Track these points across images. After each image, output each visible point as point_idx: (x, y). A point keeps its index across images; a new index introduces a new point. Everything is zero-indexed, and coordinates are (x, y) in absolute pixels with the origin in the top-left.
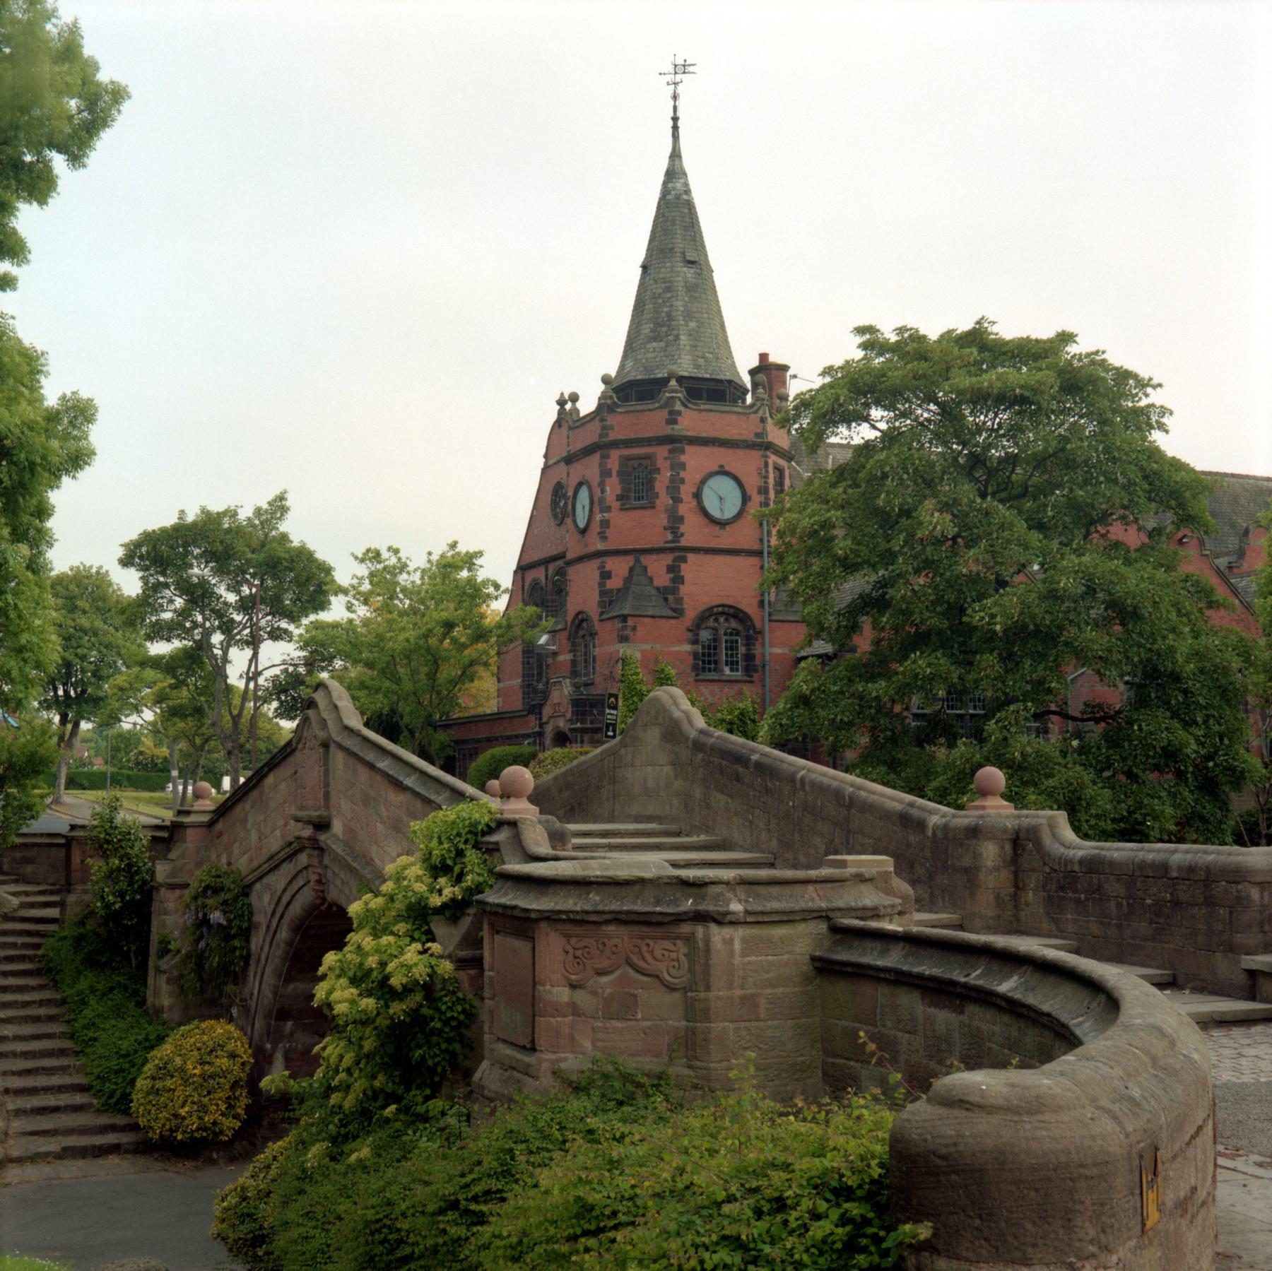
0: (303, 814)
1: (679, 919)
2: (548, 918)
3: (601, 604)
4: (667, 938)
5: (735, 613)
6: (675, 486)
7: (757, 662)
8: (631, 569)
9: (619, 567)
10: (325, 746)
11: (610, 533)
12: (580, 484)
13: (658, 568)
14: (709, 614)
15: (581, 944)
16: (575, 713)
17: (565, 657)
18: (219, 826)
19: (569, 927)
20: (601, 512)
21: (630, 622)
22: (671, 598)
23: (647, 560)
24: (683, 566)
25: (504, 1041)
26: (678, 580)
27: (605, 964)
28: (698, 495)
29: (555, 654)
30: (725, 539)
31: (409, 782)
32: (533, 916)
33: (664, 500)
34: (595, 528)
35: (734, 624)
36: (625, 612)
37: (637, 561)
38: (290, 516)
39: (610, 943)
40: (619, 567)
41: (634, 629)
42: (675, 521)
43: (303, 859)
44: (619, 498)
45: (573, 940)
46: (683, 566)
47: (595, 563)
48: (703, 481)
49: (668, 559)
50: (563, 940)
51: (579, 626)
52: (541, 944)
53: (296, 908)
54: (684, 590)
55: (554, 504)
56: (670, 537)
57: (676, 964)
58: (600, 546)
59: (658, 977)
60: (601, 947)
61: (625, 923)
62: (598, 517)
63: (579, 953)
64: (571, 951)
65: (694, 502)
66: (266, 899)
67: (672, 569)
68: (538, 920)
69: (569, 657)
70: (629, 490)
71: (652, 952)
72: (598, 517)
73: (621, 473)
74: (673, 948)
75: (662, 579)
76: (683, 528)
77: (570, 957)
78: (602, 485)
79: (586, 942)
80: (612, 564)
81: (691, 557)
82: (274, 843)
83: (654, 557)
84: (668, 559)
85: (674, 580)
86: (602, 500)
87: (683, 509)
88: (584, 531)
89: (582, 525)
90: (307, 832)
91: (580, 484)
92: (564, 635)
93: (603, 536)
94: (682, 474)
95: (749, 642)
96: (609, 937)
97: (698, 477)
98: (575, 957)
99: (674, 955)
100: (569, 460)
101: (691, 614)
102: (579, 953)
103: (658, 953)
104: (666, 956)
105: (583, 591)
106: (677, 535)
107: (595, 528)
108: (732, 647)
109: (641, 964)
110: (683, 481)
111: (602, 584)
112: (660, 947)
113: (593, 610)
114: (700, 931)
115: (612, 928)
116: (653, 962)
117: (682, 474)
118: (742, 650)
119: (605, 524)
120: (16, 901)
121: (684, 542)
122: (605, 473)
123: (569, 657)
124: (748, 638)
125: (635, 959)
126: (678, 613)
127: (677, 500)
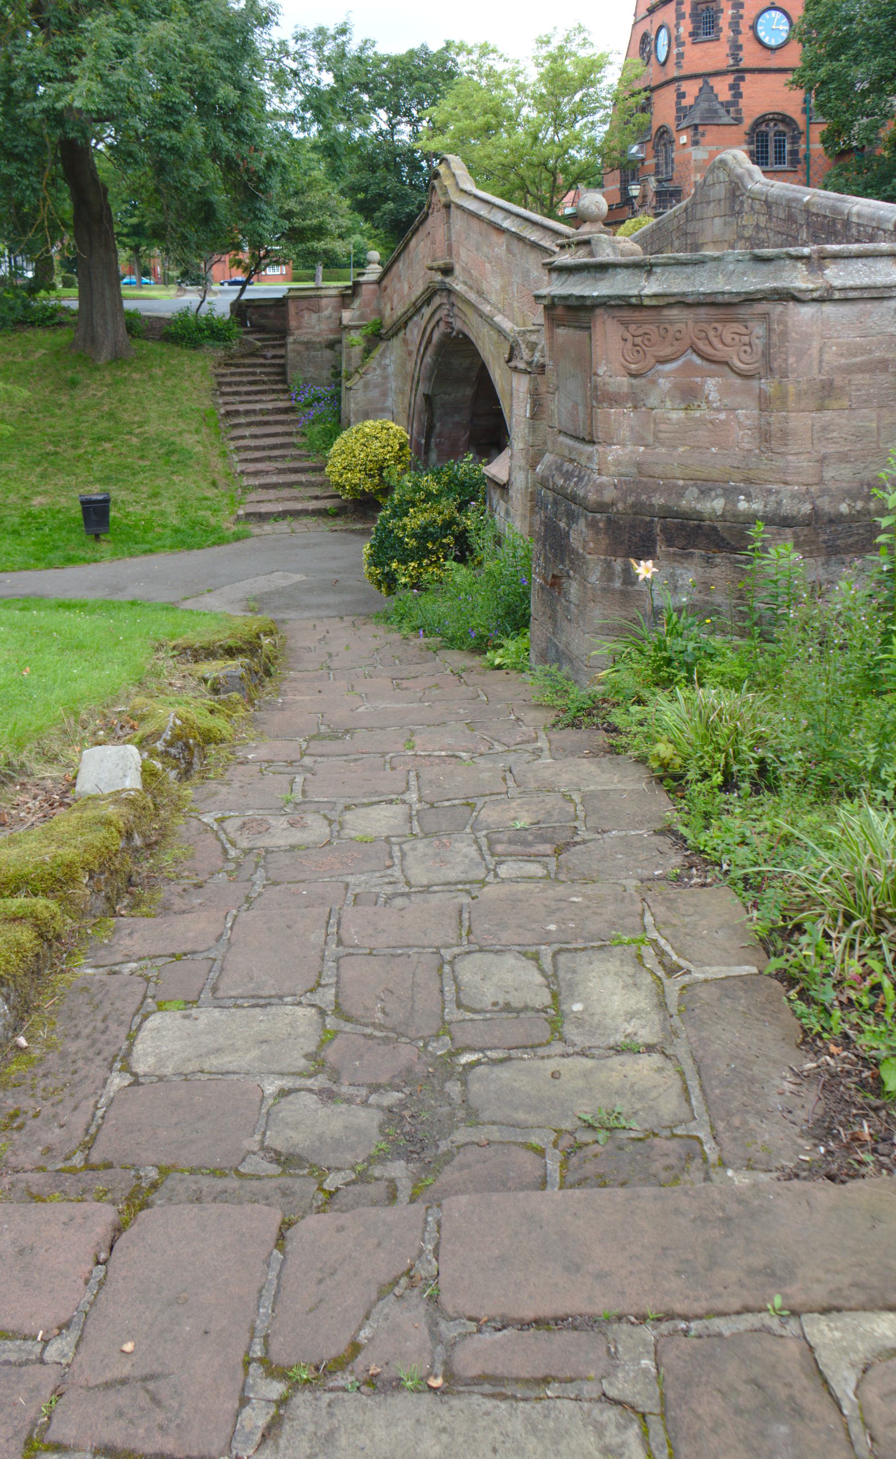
0: (435, 264)
1: (751, 299)
2: (604, 304)
3: (678, 119)
4: (737, 321)
5: (785, 119)
6: (736, 19)
7: (801, 156)
8: (701, 89)
9: (692, 88)
10: (447, 206)
11: (684, 62)
12: (661, 27)
13: (722, 88)
14: (763, 120)
15: (640, 331)
16: (659, 202)
17: (650, 162)
18: (384, 283)
19: (626, 314)
20: (678, 46)
21: (700, 129)
22: (732, 109)
23: (713, 81)
24: (742, 84)
25: (566, 434)
26: (738, 95)
27: (666, 351)
28: (753, 28)
29: (643, 160)
30: (775, 61)
31: (506, 224)
32: (588, 302)
33: (727, 33)
34: (673, 59)
35: (781, 127)
36: (697, 121)
37: (706, 83)
38: (325, 25)
39: (672, 329)
40: (692, 88)
41: (703, 135)
42: (736, 48)
43: (437, 301)
44: (692, 34)
45: (632, 327)
46: (742, 84)
47: (672, 88)
48: (759, 16)
49: (730, 79)
50: (622, 328)
51: (661, 137)
52: (598, 331)
53: (436, 337)
54: (742, 102)
55: (642, 50)
56: (731, 62)
57: (747, 348)
58: (675, 73)
59: (726, 363)
60: (663, 332)
61: (689, 305)
62: (675, 51)
63: (638, 340)
64: (630, 338)
65: (751, 33)
66: (416, 331)
67: (734, 87)
68: (594, 307)
69: (654, 161)
70: (698, 28)
71: (720, 337)
72: (675, 51)
73: (691, 16)
74: (743, 330)
75: (725, 95)
76: (741, 54)
77: (629, 345)
78: (677, 26)
79: (646, 328)
80: (685, 86)
81: (748, 76)
82: (419, 289)
83: (719, 78)
84: (730, 79)
85: (734, 96)
86: (677, 38)
87: (741, 40)
88: (664, 64)
89: (662, 58)
90: (439, 277)
91: (661, 27)
92: (650, 145)
93: (678, 65)
94: (741, 12)
95: (795, 140)
96: (671, 323)
97: (754, 14)
98: (635, 345)
99: (746, 339)
100: (651, 11)
101: (748, 122)
102: (638, 340)
103: (728, 338)
104: (735, 341)
105: (664, 110)
106: (737, 60)
107: (673, 59)
108: (780, 145)
109: (708, 350)
110: (741, 17)
111: (678, 103)
112: (729, 331)
113: (671, 124)
114: (779, 308)
115: (674, 312)
116: (720, 346)
117: (741, 12)
118: (788, 147)
119: (680, 56)
120: (259, 344)
121: (742, 65)
122: (680, 16)
123: (654, 161)
124: (793, 137)
125: (702, 346)
126: (739, 121)
127: (737, 32)
